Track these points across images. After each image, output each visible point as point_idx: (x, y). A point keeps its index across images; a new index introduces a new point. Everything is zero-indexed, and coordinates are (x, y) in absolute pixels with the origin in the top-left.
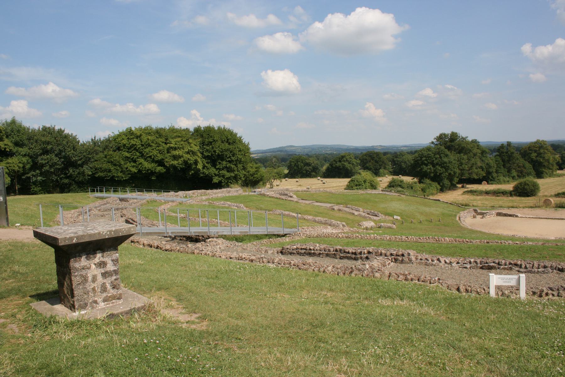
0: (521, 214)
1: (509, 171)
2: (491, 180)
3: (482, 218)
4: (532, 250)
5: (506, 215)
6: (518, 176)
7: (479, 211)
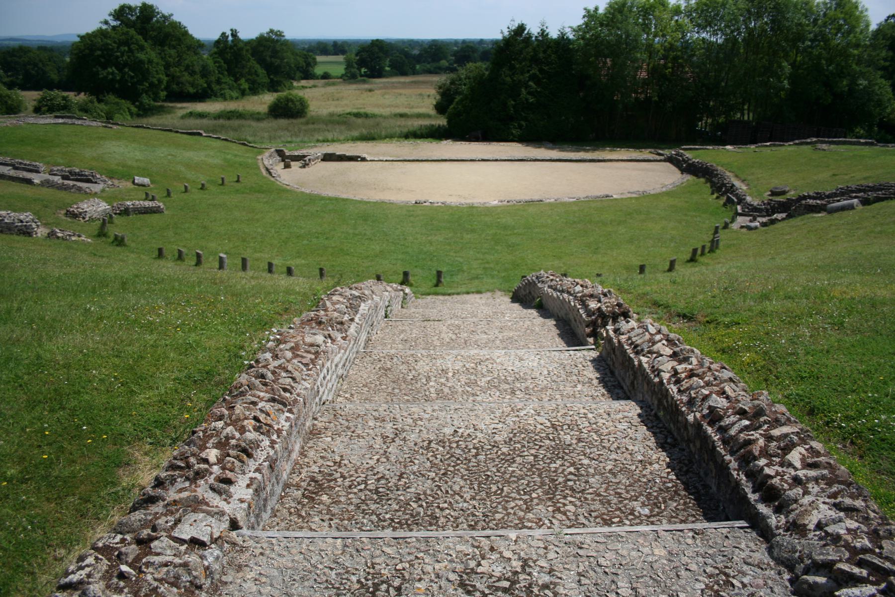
3: (304, 166)
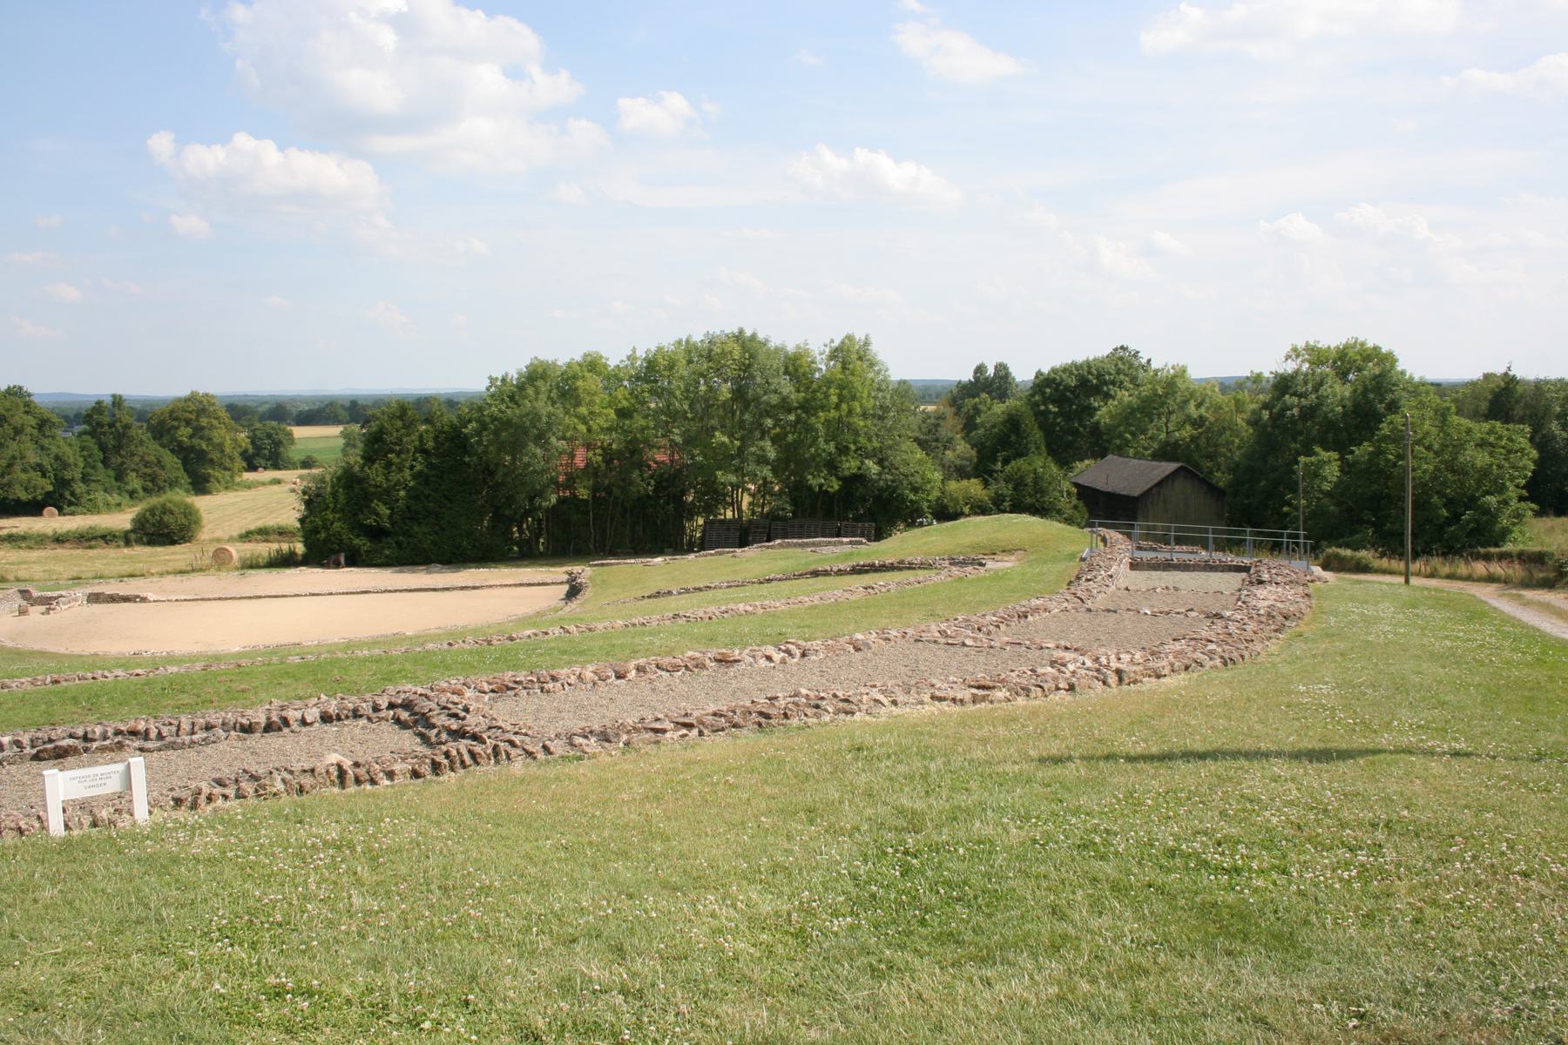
0: (155, 593)
1: (120, 476)
2: (70, 504)
4: (176, 686)
5: (113, 599)
6: (145, 489)
7: (36, 594)
